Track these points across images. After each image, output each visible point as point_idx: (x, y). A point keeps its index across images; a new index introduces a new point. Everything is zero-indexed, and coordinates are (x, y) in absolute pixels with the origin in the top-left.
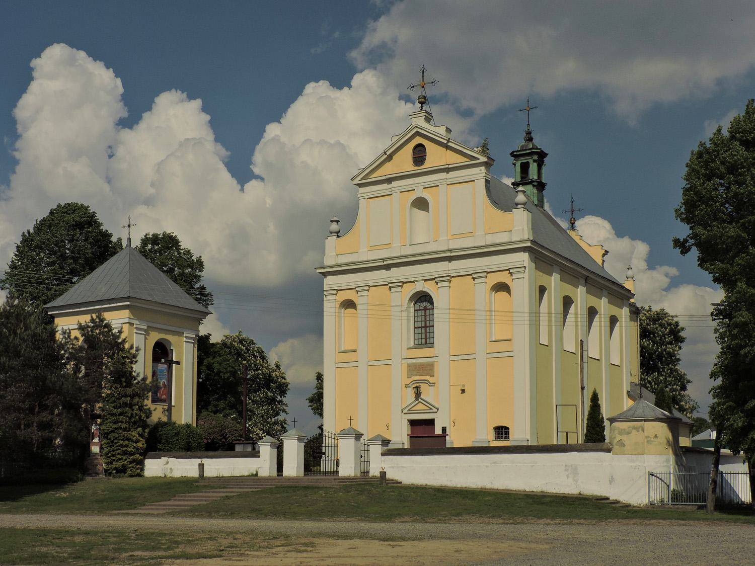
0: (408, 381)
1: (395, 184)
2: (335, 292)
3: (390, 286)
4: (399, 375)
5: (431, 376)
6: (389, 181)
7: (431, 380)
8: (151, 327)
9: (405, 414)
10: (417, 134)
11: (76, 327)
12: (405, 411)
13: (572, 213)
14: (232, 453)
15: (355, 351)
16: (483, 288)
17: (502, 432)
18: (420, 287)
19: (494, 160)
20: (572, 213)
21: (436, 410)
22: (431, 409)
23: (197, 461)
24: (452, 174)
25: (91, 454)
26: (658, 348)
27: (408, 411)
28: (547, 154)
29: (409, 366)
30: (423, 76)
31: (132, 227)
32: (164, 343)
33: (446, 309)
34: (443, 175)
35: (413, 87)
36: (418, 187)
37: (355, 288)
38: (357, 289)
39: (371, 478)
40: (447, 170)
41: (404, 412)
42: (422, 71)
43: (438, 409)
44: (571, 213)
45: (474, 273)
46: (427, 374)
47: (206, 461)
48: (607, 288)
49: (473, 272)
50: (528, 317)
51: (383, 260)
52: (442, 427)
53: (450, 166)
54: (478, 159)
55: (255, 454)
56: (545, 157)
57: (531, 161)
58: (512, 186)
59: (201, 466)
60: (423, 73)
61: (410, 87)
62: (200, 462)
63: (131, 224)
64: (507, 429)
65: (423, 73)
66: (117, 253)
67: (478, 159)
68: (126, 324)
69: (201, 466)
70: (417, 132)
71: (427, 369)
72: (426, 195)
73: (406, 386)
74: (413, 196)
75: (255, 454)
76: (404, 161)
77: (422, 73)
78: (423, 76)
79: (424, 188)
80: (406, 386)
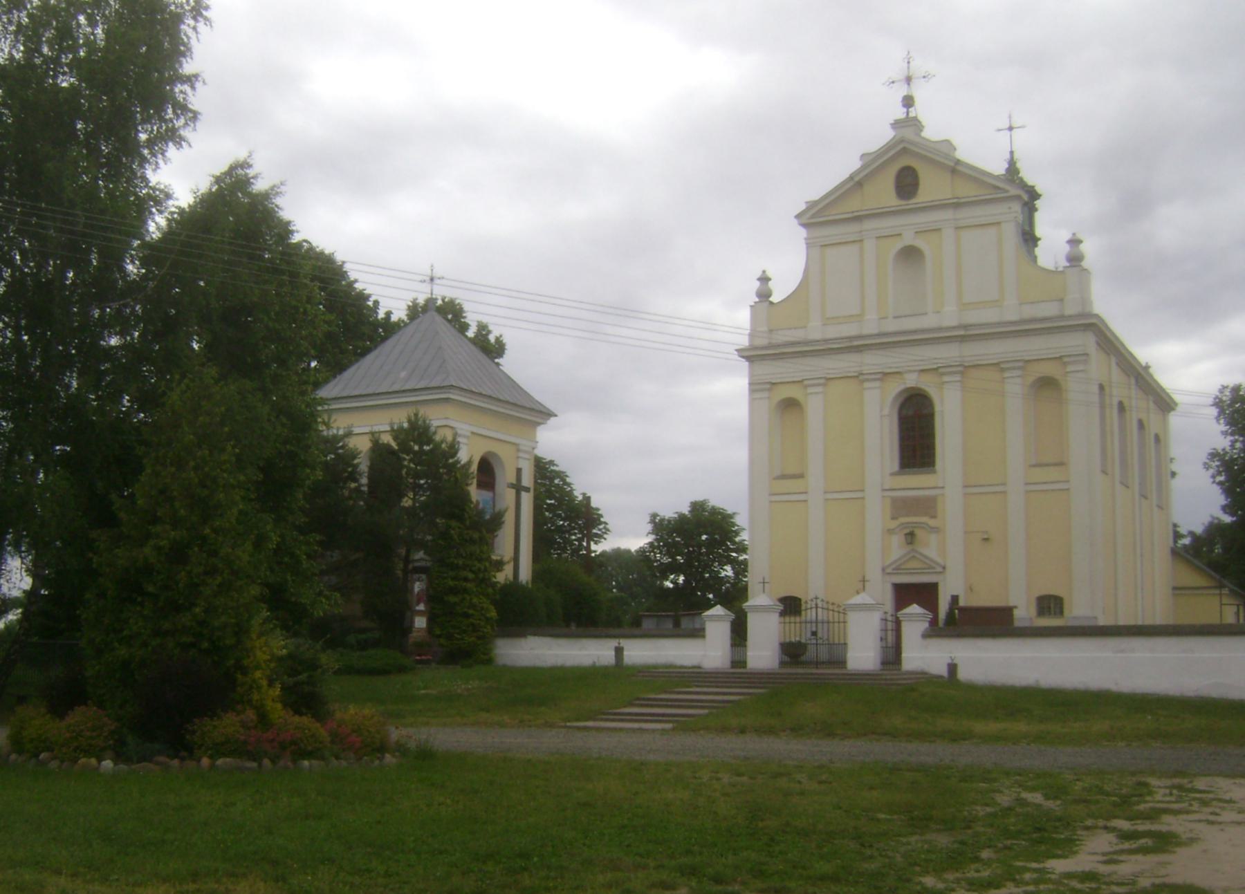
1: (868, 225)
2: (768, 386)
4: (876, 515)
6: (858, 219)
7: (932, 522)
9: (889, 574)
10: (904, 151)
11: (388, 428)
12: (889, 570)
14: (636, 631)
16: (1015, 387)
18: (911, 381)
21: (939, 569)
22: (934, 568)
23: (613, 643)
25: (414, 629)
26: (576, 524)
29: (894, 501)
33: (521, 457)
34: (948, 214)
35: (924, 77)
36: (907, 229)
38: (806, 382)
39: (905, 674)
40: (957, 205)
42: (906, 61)
43: (944, 568)
45: (806, 379)
47: (627, 644)
49: (1001, 360)
51: (851, 338)
53: (963, 200)
54: (1007, 191)
55: (698, 633)
56: (1036, 199)
59: (619, 651)
61: (930, 76)
62: (617, 645)
66: (416, 318)
69: (619, 651)
71: (927, 506)
72: (920, 243)
73: (890, 532)
74: (899, 245)
75: (698, 633)
76: (884, 193)
80: (890, 532)
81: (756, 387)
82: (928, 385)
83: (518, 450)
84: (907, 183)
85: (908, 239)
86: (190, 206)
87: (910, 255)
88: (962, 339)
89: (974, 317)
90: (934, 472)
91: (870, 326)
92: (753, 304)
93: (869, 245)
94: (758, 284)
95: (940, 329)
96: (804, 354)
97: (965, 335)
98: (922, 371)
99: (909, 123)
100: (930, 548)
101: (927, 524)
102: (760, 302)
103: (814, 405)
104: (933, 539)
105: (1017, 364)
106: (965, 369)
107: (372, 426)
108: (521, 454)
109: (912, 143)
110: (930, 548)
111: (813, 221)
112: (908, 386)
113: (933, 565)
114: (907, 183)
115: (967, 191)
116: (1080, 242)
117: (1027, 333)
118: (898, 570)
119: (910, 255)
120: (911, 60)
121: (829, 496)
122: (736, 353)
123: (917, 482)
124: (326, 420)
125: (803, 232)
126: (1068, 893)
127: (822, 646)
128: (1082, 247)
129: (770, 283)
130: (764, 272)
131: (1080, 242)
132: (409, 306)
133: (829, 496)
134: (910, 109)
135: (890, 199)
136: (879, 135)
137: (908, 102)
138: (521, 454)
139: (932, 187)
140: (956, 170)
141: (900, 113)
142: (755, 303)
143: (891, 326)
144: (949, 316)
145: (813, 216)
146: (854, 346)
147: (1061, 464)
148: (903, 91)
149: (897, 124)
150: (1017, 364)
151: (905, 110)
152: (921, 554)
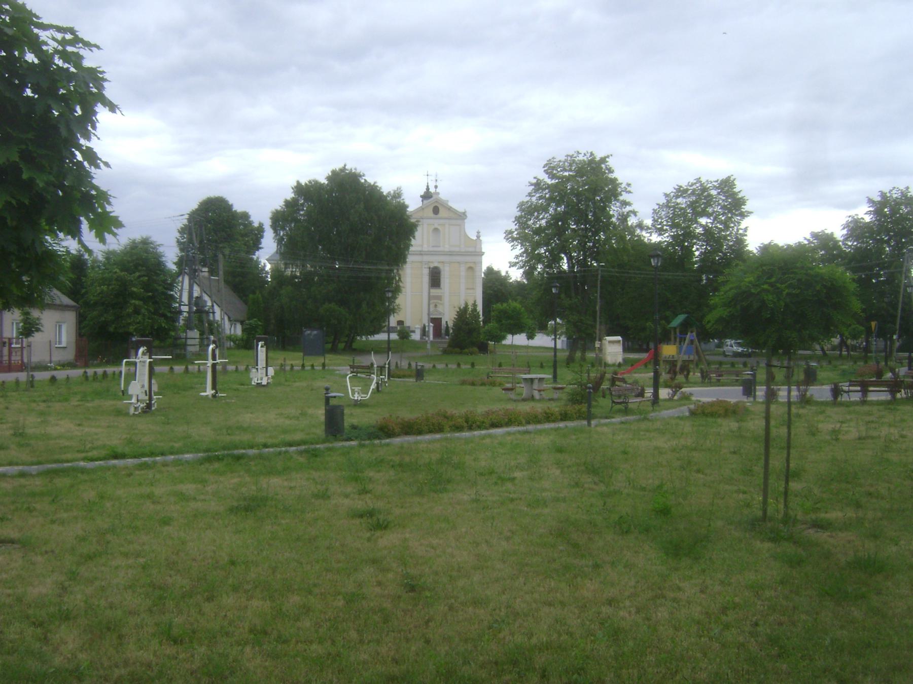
10: (436, 202)
16: (463, 269)
36: (436, 223)
71: (439, 298)
72: (439, 227)
74: (433, 227)
85: (436, 226)
86: (236, 211)
87: (436, 230)
89: (453, 249)
97: (451, 254)
100: (440, 309)
107: (863, 402)
110: (440, 309)
119: (436, 230)
123: (434, 292)
124: (844, 398)
126: (511, 683)
127: (355, 362)
132: (458, 312)
135: (431, 214)
139: (443, 213)
140: (450, 209)
143: (431, 249)
144: (447, 248)
147: (473, 289)
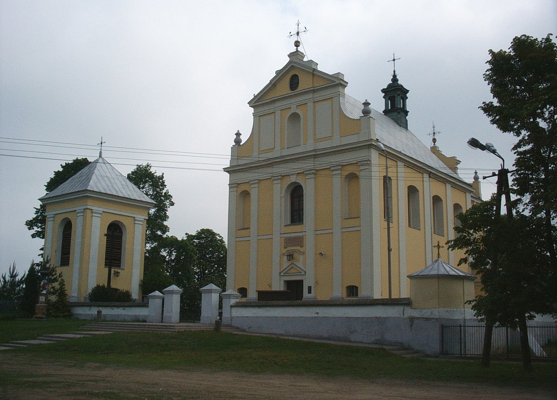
0: (284, 251)
1: (277, 104)
3: (271, 179)
4: (277, 247)
5: (301, 247)
6: (273, 102)
7: (302, 250)
8: (104, 212)
9: (282, 275)
12: (282, 274)
13: (434, 135)
15: (249, 228)
17: (352, 290)
18: (293, 179)
19: (348, 83)
20: (434, 135)
21: (304, 273)
24: (316, 95)
27: (284, 274)
28: (409, 91)
30: (298, 28)
31: (100, 143)
32: (120, 225)
34: (310, 96)
36: (293, 105)
37: (249, 182)
38: (251, 182)
40: (314, 91)
41: (281, 274)
42: (297, 24)
43: (305, 272)
44: (433, 135)
46: (298, 245)
48: (450, 182)
50: (230, 156)
52: (308, 287)
53: (316, 88)
54: (335, 82)
57: (396, 95)
58: (383, 114)
60: (298, 25)
63: (103, 142)
64: (357, 288)
65: (298, 25)
67: (335, 82)
68: (131, 218)
70: (292, 66)
71: (298, 241)
72: (298, 111)
76: (284, 88)
77: (297, 26)
78: (298, 28)
79: (297, 106)
81: (232, 185)
82: (300, 180)
83: (135, 220)
84: (294, 83)
87: (295, 117)
88: (315, 156)
90: (303, 224)
91: (276, 154)
92: (232, 146)
93: (278, 113)
94: (235, 136)
95: (359, 142)
96: (257, 167)
97: (315, 155)
98: (298, 174)
99: (295, 56)
101: (299, 250)
102: (236, 145)
103: (254, 193)
104: (301, 258)
105: (256, 182)
106: (316, 172)
108: (136, 222)
109: (295, 63)
111: (255, 104)
112: (292, 181)
113: (301, 271)
114: (294, 83)
115: (319, 83)
116: (369, 104)
117: (286, 161)
118: (286, 274)
120: (299, 24)
121: (344, 230)
122: (223, 170)
123: (297, 228)
125: (252, 110)
128: (241, 137)
129: (241, 136)
130: (238, 131)
131: (369, 104)
133: (344, 230)
134: (298, 48)
136: (283, 61)
137: (297, 44)
138: (136, 222)
139: (305, 83)
141: (294, 49)
142: (233, 145)
143: (286, 152)
145: (256, 102)
146: (271, 163)
148: (295, 38)
149: (290, 55)
150: (256, 182)
151: (296, 48)
152: (296, 266)
